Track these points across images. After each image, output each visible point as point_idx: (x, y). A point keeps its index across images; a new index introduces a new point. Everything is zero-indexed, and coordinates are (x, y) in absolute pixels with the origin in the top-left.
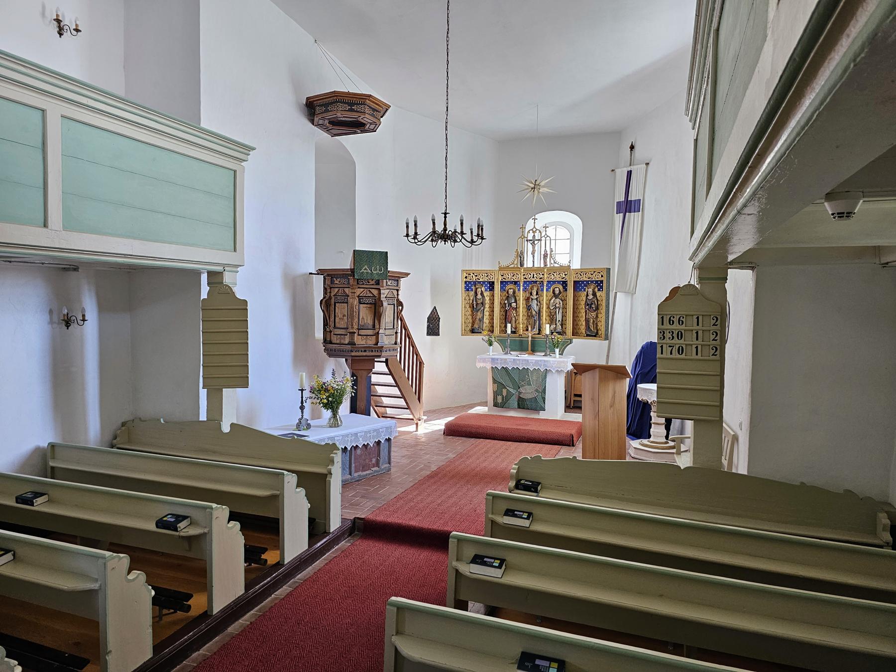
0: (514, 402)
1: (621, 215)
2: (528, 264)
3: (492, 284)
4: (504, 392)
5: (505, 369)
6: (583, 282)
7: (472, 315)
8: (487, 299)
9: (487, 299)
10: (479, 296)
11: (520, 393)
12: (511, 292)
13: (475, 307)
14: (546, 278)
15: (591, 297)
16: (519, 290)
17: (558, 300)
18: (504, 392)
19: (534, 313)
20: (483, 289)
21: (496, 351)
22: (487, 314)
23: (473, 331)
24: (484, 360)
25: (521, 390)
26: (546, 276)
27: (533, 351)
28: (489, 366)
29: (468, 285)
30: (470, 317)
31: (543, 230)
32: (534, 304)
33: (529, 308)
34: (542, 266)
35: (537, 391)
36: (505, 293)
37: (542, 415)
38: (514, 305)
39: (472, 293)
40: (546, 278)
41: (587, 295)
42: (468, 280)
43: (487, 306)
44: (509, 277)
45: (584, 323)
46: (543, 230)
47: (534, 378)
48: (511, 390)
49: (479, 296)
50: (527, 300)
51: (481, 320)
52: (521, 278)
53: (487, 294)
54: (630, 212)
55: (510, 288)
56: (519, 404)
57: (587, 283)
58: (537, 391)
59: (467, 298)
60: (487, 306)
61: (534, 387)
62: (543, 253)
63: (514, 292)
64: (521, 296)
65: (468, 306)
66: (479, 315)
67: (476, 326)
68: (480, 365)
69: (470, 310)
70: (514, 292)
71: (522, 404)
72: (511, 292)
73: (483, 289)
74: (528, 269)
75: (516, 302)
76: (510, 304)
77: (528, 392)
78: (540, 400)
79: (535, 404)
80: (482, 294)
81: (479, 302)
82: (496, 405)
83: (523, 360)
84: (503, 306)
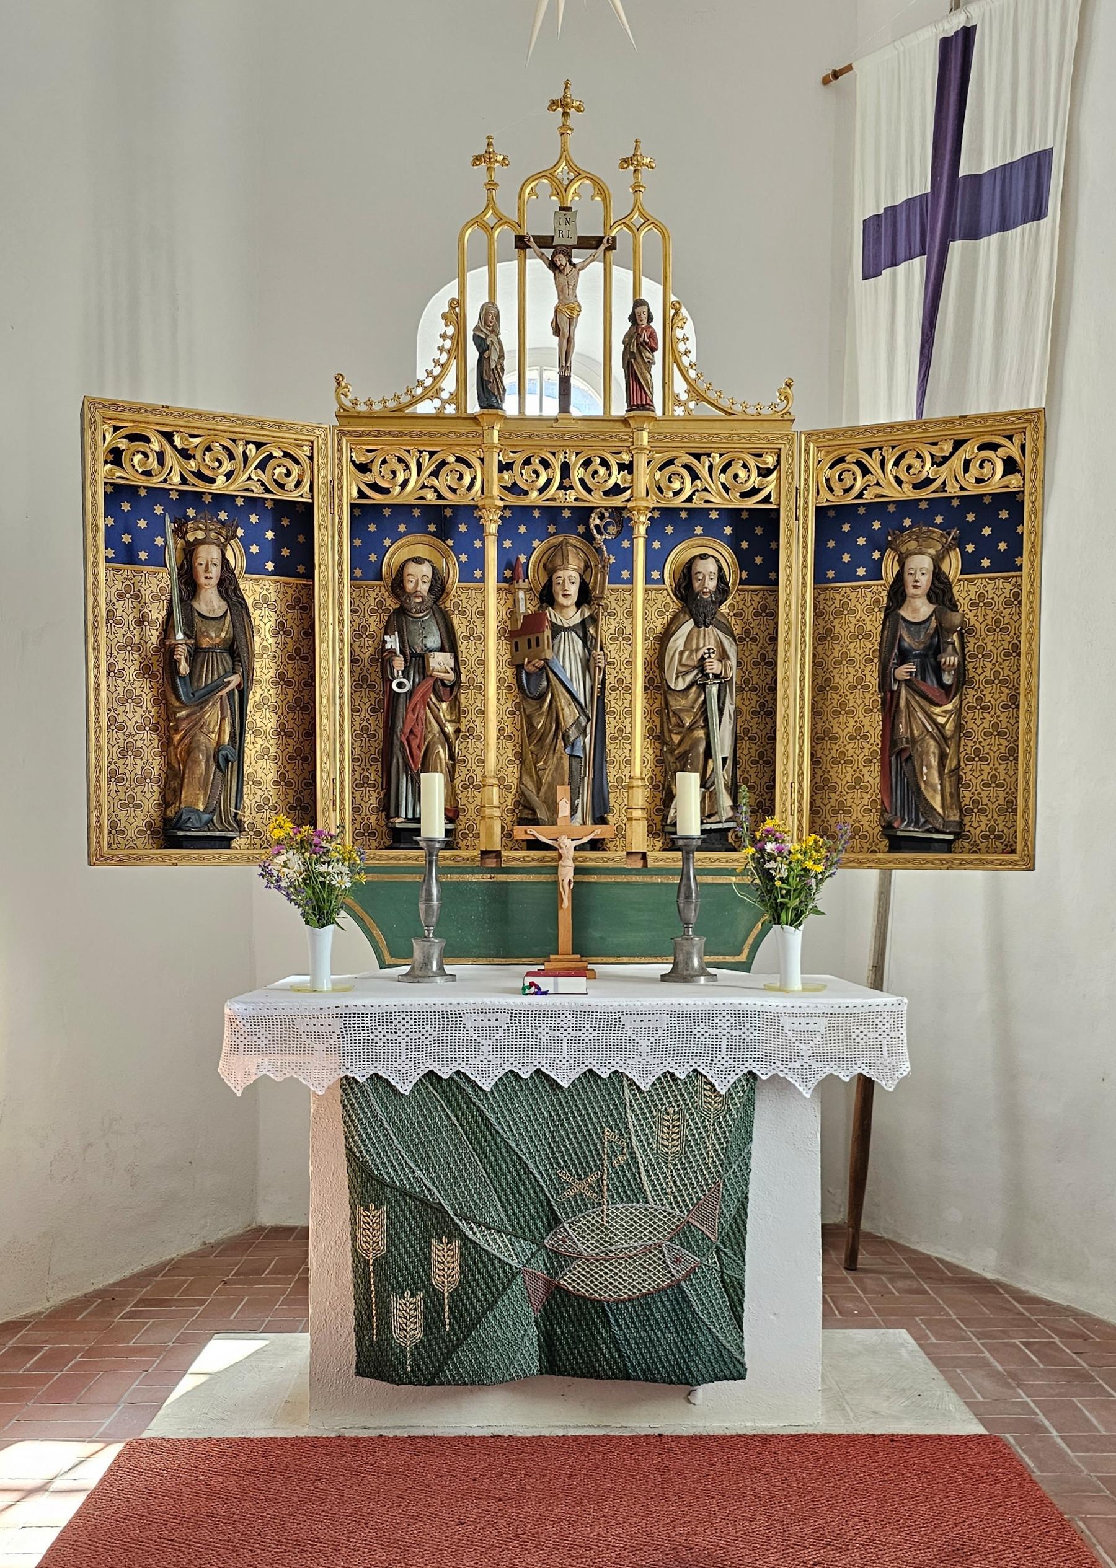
0: (516, 1327)
1: (914, 270)
2: (532, 398)
3: (294, 523)
4: (445, 1265)
5: (453, 1090)
6: (878, 509)
7: (166, 725)
8: (264, 627)
9: (264, 627)
10: (210, 602)
11: (559, 1260)
12: (419, 578)
13: (187, 673)
14: (644, 492)
15: (919, 609)
16: (472, 569)
17: (711, 636)
18: (445, 1265)
19: (569, 714)
20: (235, 557)
21: (337, 964)
22: (264, 718)
23: (171, 833)
24: (282, 1033)
25: (573, 1234)
26: (643, 477)
27: (585, 954)
28: (319, 1075)
29: (133, 517)
30: (148, 742)
31: (619, 182)
32: (568, 657)
33: (531, 684)
34: (619, 408)
35: (685, 1235)
36: (378, 592)
37: (716, 1410)
38: (440, 662)
39: (157, 583)
40: (644, 492)
41: (898, 593)
42: (129, 475)
43: (265, 670)
44: (410, 486)
45: (872, 775)
46: (619, 182)
47: (668, 1142)
48: (498, 1246)
49: (210, 602)
50: (524, 635)
51: (229, 759)
52: (484, 487)
53: (261, 592)
54: (973, 233)
55: (414, 557)
56: (548, 1345)
57: (891, 522)
58: (685, 1235)
59: (126, 610)
60: (265, 670)
61: (661, 1208)
62: (621, 327)
63: (439, 587)
64: (487, 610)
65: (130, 665)
66: (215, 721)
67: (195, 798)
68: (239, 1071)
69: (145, 691)
70: (439, 587)
71: (578, 1343)
72: (419, 578)
73: (235, 557)
74: (523, 428)
75: (450, 644)
76: (418, 662)
77: (619, 1254)
78: (706, 1302)
79: (689, 1339)
80: (228, 586)
81: (214, 637)
82: (376, 1361)
83: (581, 1016)
84: (370, 671)
